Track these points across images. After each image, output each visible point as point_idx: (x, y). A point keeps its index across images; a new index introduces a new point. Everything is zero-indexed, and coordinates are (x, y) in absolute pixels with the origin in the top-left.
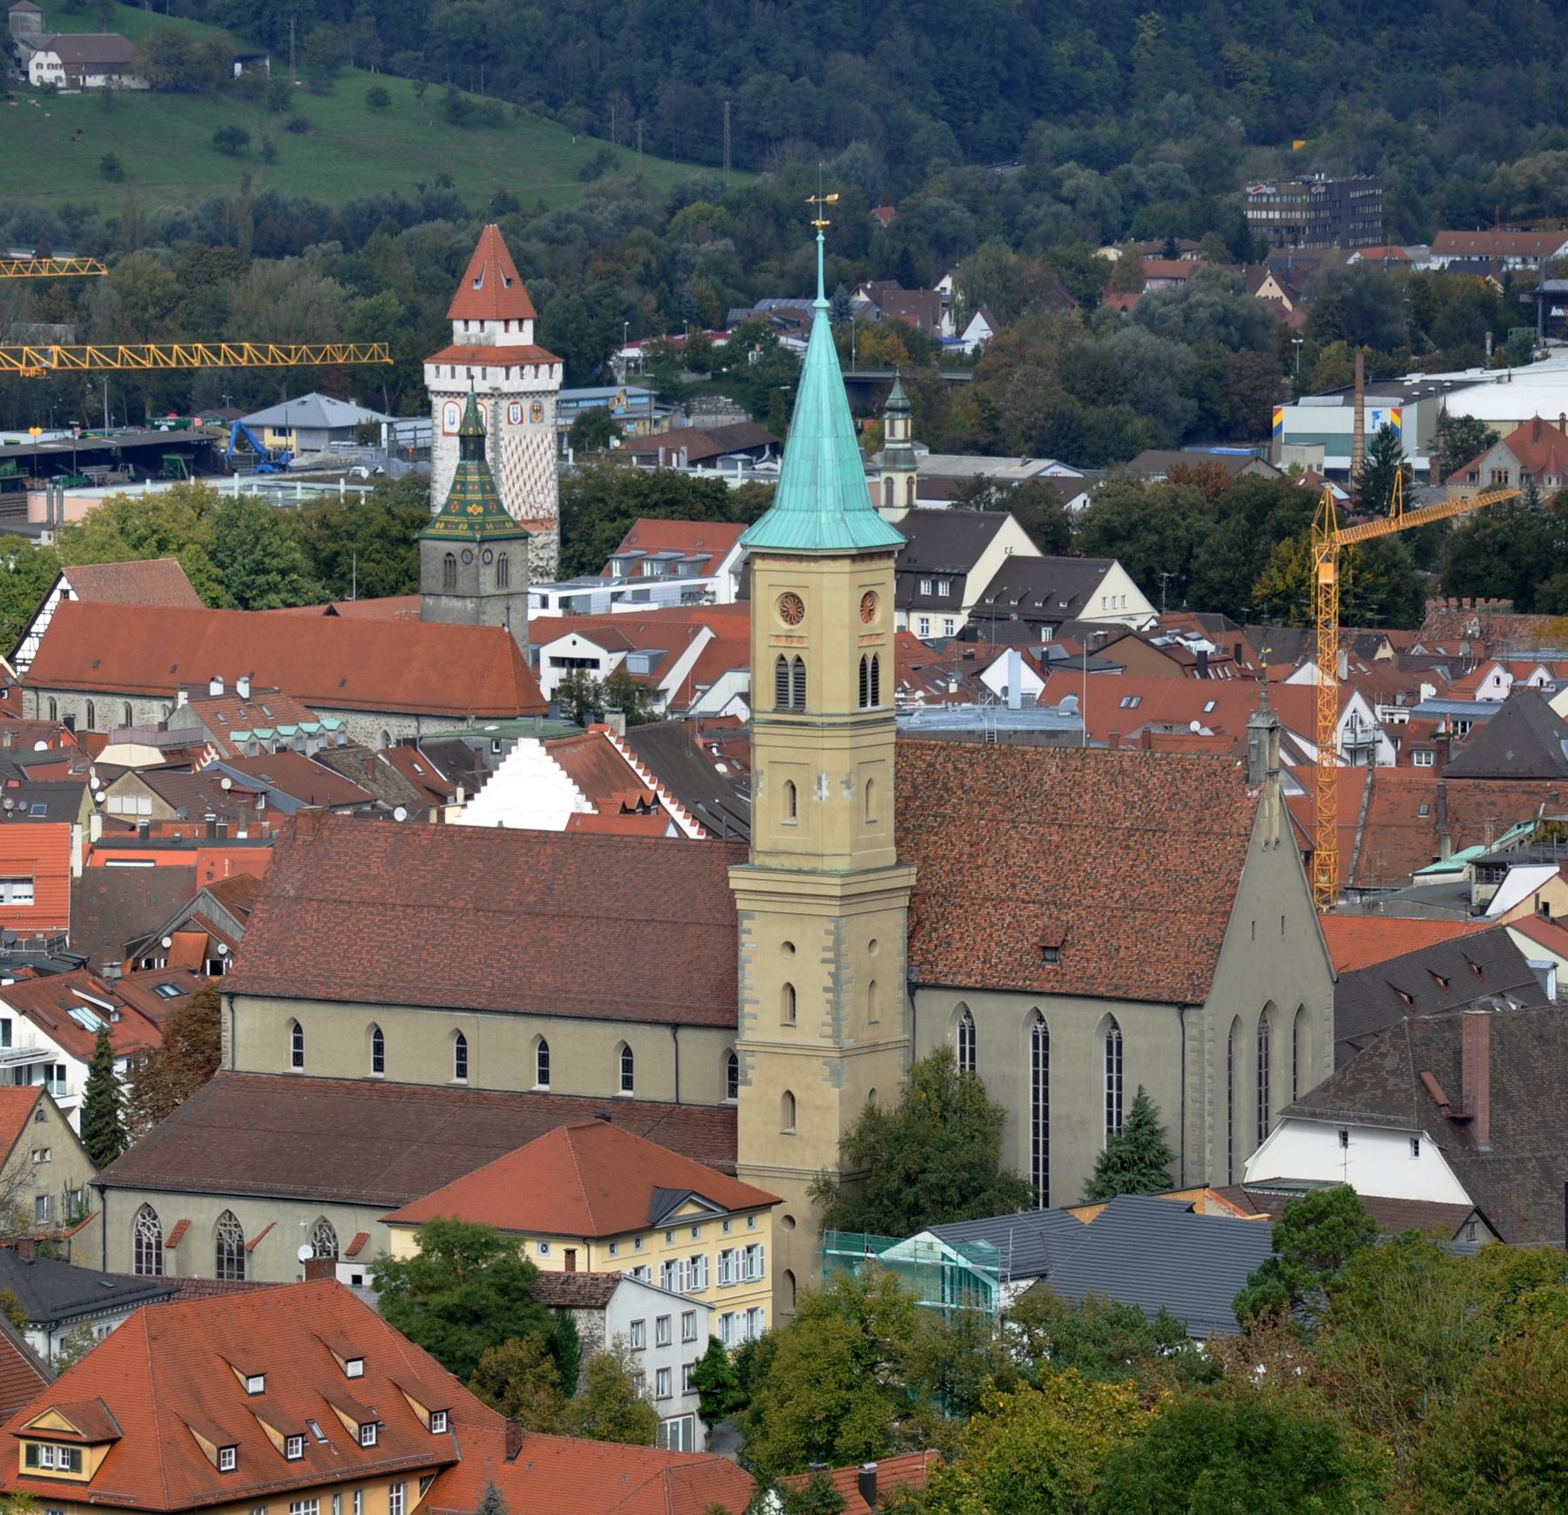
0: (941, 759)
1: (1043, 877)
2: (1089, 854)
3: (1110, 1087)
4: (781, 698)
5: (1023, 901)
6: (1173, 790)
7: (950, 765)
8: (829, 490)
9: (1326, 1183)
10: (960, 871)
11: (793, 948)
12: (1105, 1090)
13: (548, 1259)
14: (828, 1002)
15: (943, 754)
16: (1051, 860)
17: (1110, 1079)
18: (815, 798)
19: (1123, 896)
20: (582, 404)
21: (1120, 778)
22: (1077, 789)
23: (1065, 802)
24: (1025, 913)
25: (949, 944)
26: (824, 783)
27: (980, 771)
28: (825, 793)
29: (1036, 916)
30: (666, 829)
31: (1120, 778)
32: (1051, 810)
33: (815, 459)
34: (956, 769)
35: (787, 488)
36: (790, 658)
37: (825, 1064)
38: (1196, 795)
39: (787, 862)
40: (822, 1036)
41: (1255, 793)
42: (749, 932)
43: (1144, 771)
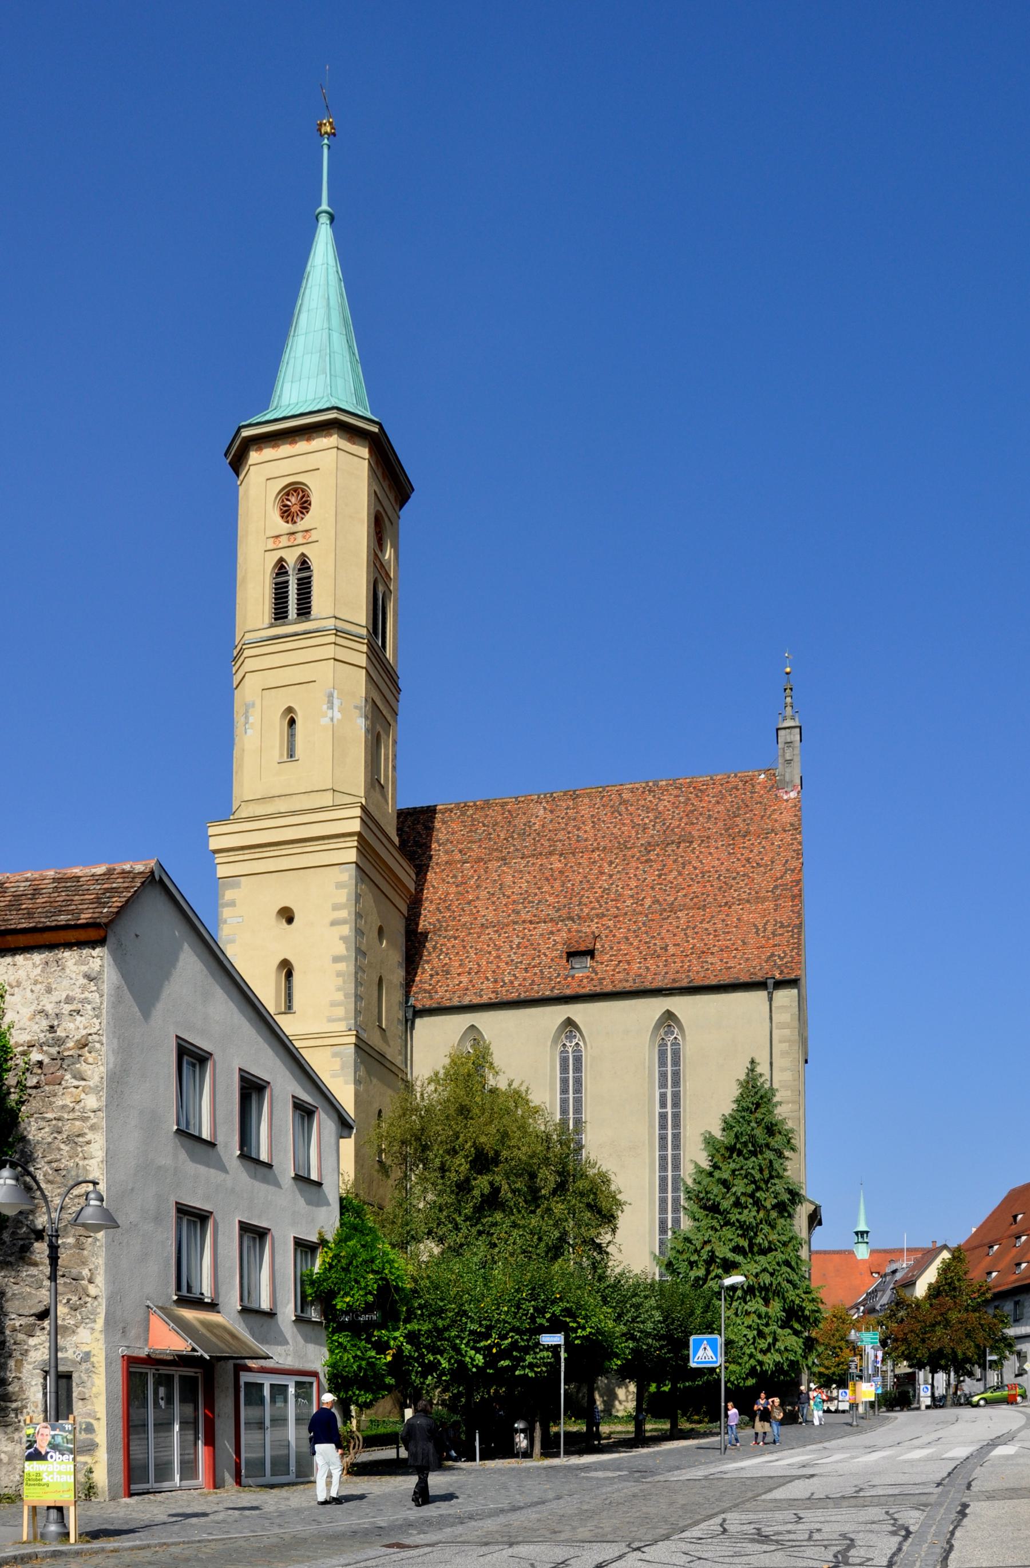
1: (551, 899)
2: (602, 873)
3: (663, 1105)
4: (280, 614)
5: (531, 922)
6: (690, 808)
11: (290, 920)
13: (315, 1410)
14: (339, 974)
17: (663, 1096)
19: (656, 901)
20: (173, 1549)
21: (622, 808)
23: (561, 835)
24: (539, 931)
25: (448, 972)
26: (336, 703)
29: (552, 933)
31: (622, 808)
32: (547, 844)
36: (291, 559)
37: (335, 1055)
38: (721, 808)
39: (283, 806)
40: (331, 1020)
42: (232, 904)
43: (650, 798)
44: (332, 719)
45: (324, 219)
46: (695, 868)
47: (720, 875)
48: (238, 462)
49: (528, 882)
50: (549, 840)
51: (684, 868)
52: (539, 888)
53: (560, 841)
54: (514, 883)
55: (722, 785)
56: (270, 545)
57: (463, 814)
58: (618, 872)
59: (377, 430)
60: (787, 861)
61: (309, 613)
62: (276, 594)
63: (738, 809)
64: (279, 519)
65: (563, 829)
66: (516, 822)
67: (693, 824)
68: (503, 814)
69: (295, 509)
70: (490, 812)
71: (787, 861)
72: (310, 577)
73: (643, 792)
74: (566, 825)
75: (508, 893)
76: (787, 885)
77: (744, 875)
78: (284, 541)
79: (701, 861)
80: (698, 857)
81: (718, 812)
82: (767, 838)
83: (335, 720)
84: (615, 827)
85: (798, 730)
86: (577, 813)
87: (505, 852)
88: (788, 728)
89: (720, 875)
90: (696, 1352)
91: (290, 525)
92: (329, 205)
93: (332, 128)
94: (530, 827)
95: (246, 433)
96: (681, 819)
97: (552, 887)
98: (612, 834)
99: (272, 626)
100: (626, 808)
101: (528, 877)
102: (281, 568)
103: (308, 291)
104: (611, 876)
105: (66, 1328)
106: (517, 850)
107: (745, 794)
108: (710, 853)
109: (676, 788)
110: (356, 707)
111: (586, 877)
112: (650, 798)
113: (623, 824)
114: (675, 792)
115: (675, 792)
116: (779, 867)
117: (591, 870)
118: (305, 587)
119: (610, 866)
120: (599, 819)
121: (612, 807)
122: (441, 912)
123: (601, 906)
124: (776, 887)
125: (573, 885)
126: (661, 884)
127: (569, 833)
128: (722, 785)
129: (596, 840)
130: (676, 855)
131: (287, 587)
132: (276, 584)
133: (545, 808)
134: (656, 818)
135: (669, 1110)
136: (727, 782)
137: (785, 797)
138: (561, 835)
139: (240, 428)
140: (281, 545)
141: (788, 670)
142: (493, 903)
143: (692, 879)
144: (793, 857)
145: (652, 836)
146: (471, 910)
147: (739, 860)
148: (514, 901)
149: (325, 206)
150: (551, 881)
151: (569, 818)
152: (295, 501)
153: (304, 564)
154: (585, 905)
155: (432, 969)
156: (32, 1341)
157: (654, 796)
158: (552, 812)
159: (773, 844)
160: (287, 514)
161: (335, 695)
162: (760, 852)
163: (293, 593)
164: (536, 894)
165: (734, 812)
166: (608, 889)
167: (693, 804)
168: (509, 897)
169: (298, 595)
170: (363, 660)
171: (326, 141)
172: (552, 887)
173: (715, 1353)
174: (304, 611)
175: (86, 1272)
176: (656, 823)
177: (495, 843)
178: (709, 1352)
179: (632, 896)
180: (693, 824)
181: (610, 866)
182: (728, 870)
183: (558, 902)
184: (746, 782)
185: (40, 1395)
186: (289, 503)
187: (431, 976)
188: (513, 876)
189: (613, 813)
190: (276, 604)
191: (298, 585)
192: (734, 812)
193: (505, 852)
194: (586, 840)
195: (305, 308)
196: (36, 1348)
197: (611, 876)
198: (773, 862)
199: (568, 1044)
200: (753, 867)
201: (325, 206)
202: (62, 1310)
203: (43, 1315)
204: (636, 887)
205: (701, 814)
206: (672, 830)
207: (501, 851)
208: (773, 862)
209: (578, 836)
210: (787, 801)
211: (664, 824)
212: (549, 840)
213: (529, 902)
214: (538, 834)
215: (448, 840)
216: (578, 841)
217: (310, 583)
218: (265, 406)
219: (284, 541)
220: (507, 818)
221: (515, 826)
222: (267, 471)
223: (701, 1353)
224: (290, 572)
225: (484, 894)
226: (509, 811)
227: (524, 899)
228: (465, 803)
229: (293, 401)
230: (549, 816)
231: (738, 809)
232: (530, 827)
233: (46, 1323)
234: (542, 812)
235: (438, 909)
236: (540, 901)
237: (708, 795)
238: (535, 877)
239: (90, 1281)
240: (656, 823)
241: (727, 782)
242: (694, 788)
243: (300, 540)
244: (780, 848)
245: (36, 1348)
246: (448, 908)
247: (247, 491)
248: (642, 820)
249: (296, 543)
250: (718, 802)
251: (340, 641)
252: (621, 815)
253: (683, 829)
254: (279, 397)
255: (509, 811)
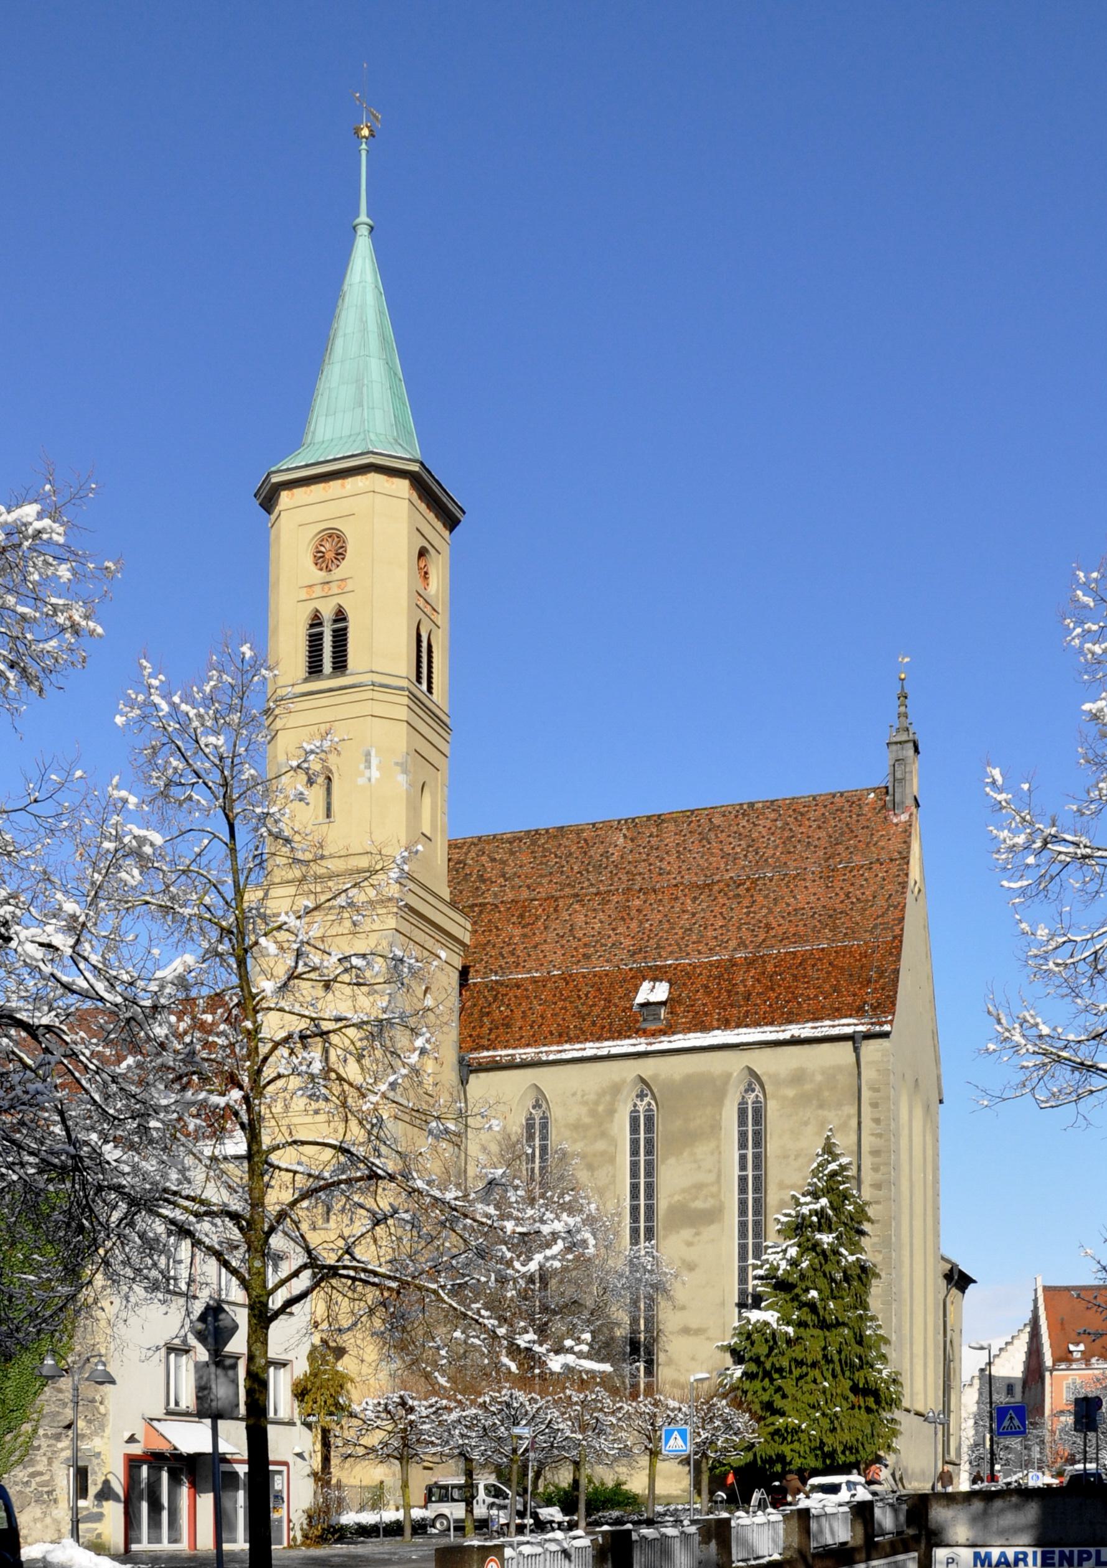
0: (472, 854)
4: (314, 668)
6: (787, 834)
7: (484, 858)
8: (378, 414)
9: (249, 1321)
10: (512, 953)
12: (736, 1172)
15: (474, 849)
16: (634, 925)
18: (362, 781)
21: (712, 835)
22: (655, 853)
23: (642, 867)
26: (374, 761)
27: (525, 858)
28: (375, 774)
30: (234, 1556)
31: (712, 835)
32: (624, 878)
33: (359, 383)
34: (493, 860)
35: (322, 419)
36: (328, 614)
38: (822, 834)
41: (904, 817)
42: (343, 486)
43: (744, 823)
44: (370, 780)
45: (363, 231)
46: (788, 905)
47: (815, 913)
48: (268, 499)
49: (601, 922)
50: (627, 873)
51: (775, 904)
52: (614, 929)
53: (640, 874)
54: (586, 923)
55: (825, 806)
56: (304, 596)
57: (534, 843)
58: (703, 910)
59: (417, 469)
60: (890, 895)
61: (345, 666)
62: (310, 647)
63: (842, 834)
64: (313, 568)
65: (644, 860)
66: (592, 853)
67: (790, 853)
68: (578, 843)
69: (330, 555)
70: (564, 842)
71: (890, 895)
72: (345, 629)
73: (736, 816)
74: (648, 855)
75: (580, 934)
76: (888, 923)
77: (841, 913)
78: (318, 591)
79: (794, 897)
80: (792, 891)
81: (819, 839)
82: (870, 868)
83: (373, 780)
84: (702, 857)
85: (911, 745)
86: (661, 841)
87: (578, 887)
88: (900, 743)
89: (815, 913)
90: (667, 1443)
91: (323, 573)
92: (368, 216)
93: (371, 131)
94: (607, 858)
95: (275, 479)
96: (776, 847)
97: (628, 927)
98: (699, 865)
99: (306, 680)
100: (716, 835)
101: (601, 916)
102: (316, 621)
103: (344, 313)
104: (694, 915)
105: (84, 1436)
106: (592, 885)
107: (850, 817)
108: (806, 887)
109: (774, 810)
110: (397, 764)
111: (666, 916)
112: (744, 823)
113: (712, 854)
114: (773, 816)
115: (773, 816)
116: (881, 902)
117: (673, 907)
118: (340, 638)
119: (694, 903)
120: (685, 848)
121: (700, 834)
122: (504, 958)
123: (681, 949)
124: (875, 927)
125: (651, 925)
126: (749, 923)
127: (650, 865)
128: (825, 806)
129: (680, 872)
130: (768, 889)
131: (321, 639)
132: (310, 636)
133: (625, 836)
134: (749, 846)
135: (750, 1173)
136: (832, 803)
137: (895, 821)
138: (642, 867)
139: (268, 475)
140: (314, 596)
141: (903, 676)
142: (563, 946)
143: (783, 917)
144: (897, 891)
145: (743, 868)
146: (537, 955)
147: (837, 894)
148: (585, 945)
149: (363, 218)
150: (628, 921)
151: (652, 847)
152: (331, 550)
153: (340, 616)
154: (664, 948)
155: (492, 1023)
156: (60, 1445)
157: (748, 821)
158: (632, 840)
159: (877, 876)
160: (319, 559)
161: (373, 753)
162: (862, 886)
163: (329, 647)
164: (609, 937)
165: (836, 839)
166: (690, 930)
167: (791, 830)
168: (579, 940)
169: (334, 647)
170: (403, 713)
171: (364, 146)
172: (628, 927)
173: (685, 1444)
174: (340, 664)
175: (98, 1398)
176: (748, 852)
177: (568, 877)
178: (680, 1442)
179: (716, 938)
180: (790, 853)
181: (694, 903)
182: (824, 907)
183: (634, 945)
184: (853, 803)
185: (65, 1482)
186: (323, 549)
187: (491, 1030)
188: (586, 916)
189: (700, 841)
190: (310, 657)
191: (334, 637)
192: (836, 839)
193: (578, 887)
194: (669, 873)
195: (340, 333)
196: (62, 1450)
197: (694, 915)
198: (874, 897)
199: (639, 1103)
200: (852, 903)
201: (363, 218)
202: (81, 1424)
203: (69, 1427)
204: (721, 927)
205: (799, 841)
206: (766, 860)
207: (574, 886)
208: (874, 897)
209: (661, 869)
210: (897, 825)
211: (757, 853)
212: (627, 873)
213: (602, 945)
214: (616, 866)
215: (515, 874)
216: (660, 874)
217: (346, 634)
218: (296, 438)
219: (318, 591)
220: (582, 847)
221: (591, 857)
222: (301, 514)
223: (672, 1442)
224: (325, 624)
225: (551, 936)
226: (585, 840)
227: (597, 942)
228: (537, 831)
229: (328, 437)
230: (630, 845)
231: (842, 834)
232: (607, 858)
233: (70, 1433)
234: (621, 840)
235: (501, 954)
236: (613, 944)
237: (809, 819)
238: (610, 916)
239: (101, 1403)
240: (748, 852)
241: (832, 803)
242: (794, 810)
243: (335, 590)
244: (884, 880)
245: (62, 1450)
246: (512, 953)
247: (278, 537)
248: (733, 848)
249: (331, 593)
250: (820, 828)
251: (377, 695)
252: (709, 843)
253: (778, 858)
254: (314, 433)
255: (585, 840)
